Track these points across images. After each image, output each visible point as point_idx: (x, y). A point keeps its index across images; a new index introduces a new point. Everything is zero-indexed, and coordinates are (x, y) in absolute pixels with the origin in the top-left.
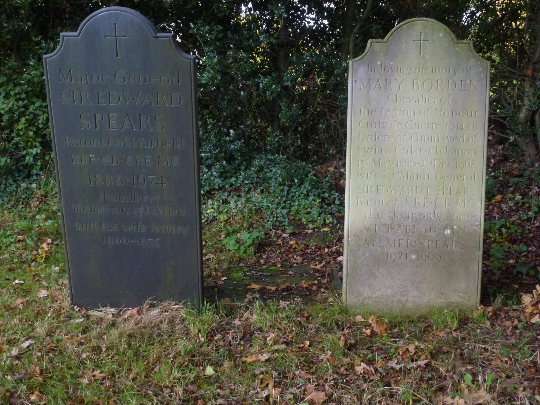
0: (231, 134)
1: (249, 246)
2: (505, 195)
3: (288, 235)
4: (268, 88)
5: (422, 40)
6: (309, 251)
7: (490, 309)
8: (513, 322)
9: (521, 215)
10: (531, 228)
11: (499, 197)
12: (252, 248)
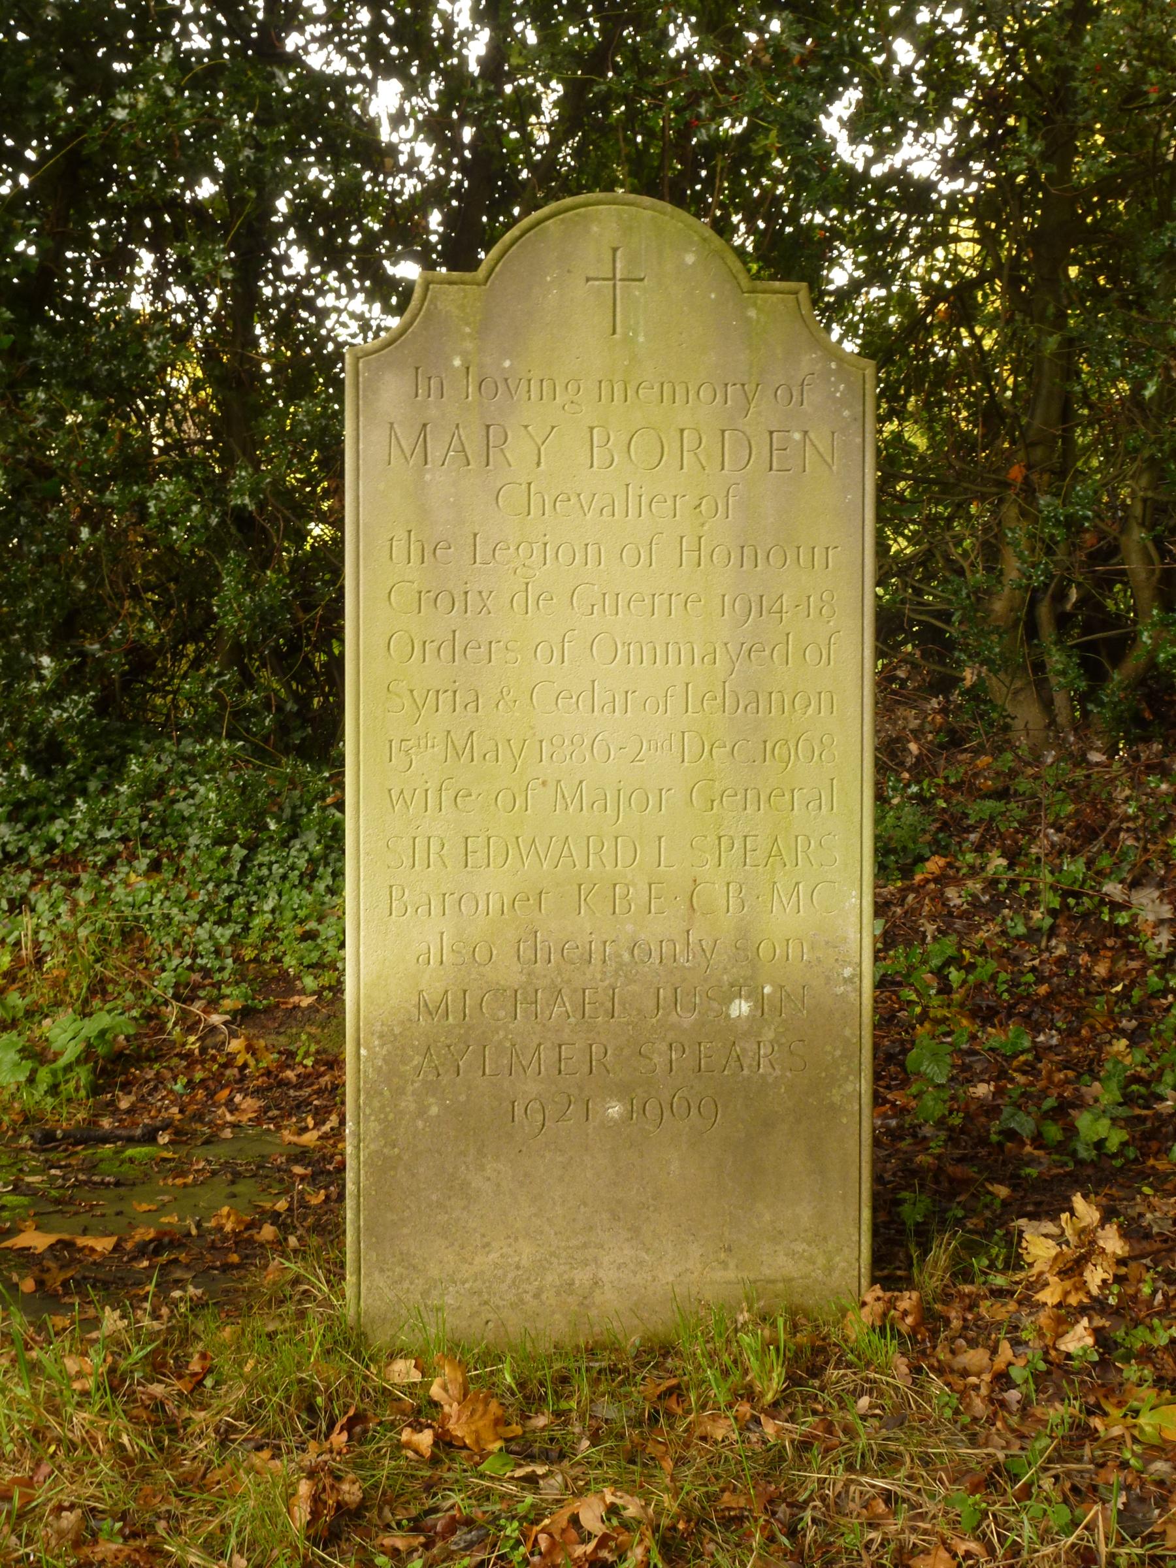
0: (46, 672)
1: (68, 1068)
2: (955, 857)
3: (228, 1017)
4: (176, 514)
5: (618, 276)
6: (290, 1074)
7: (908, 1300)
8: (994, 1351)
9: (1009, 922)
10: (1042, 962)
11: (935, 864)
12: (83, 1074)
